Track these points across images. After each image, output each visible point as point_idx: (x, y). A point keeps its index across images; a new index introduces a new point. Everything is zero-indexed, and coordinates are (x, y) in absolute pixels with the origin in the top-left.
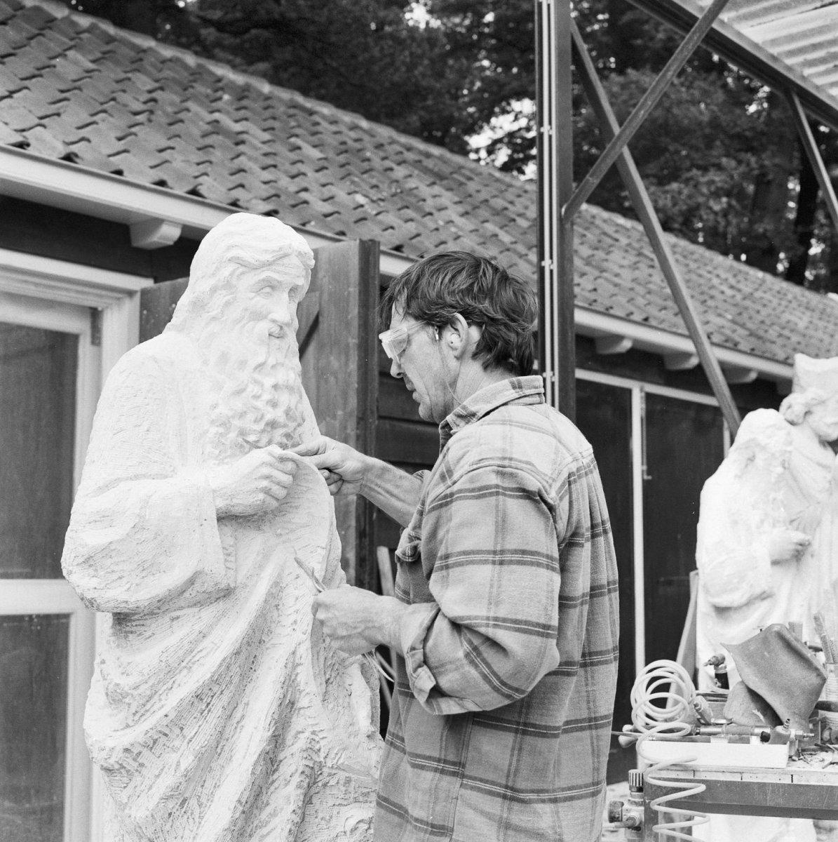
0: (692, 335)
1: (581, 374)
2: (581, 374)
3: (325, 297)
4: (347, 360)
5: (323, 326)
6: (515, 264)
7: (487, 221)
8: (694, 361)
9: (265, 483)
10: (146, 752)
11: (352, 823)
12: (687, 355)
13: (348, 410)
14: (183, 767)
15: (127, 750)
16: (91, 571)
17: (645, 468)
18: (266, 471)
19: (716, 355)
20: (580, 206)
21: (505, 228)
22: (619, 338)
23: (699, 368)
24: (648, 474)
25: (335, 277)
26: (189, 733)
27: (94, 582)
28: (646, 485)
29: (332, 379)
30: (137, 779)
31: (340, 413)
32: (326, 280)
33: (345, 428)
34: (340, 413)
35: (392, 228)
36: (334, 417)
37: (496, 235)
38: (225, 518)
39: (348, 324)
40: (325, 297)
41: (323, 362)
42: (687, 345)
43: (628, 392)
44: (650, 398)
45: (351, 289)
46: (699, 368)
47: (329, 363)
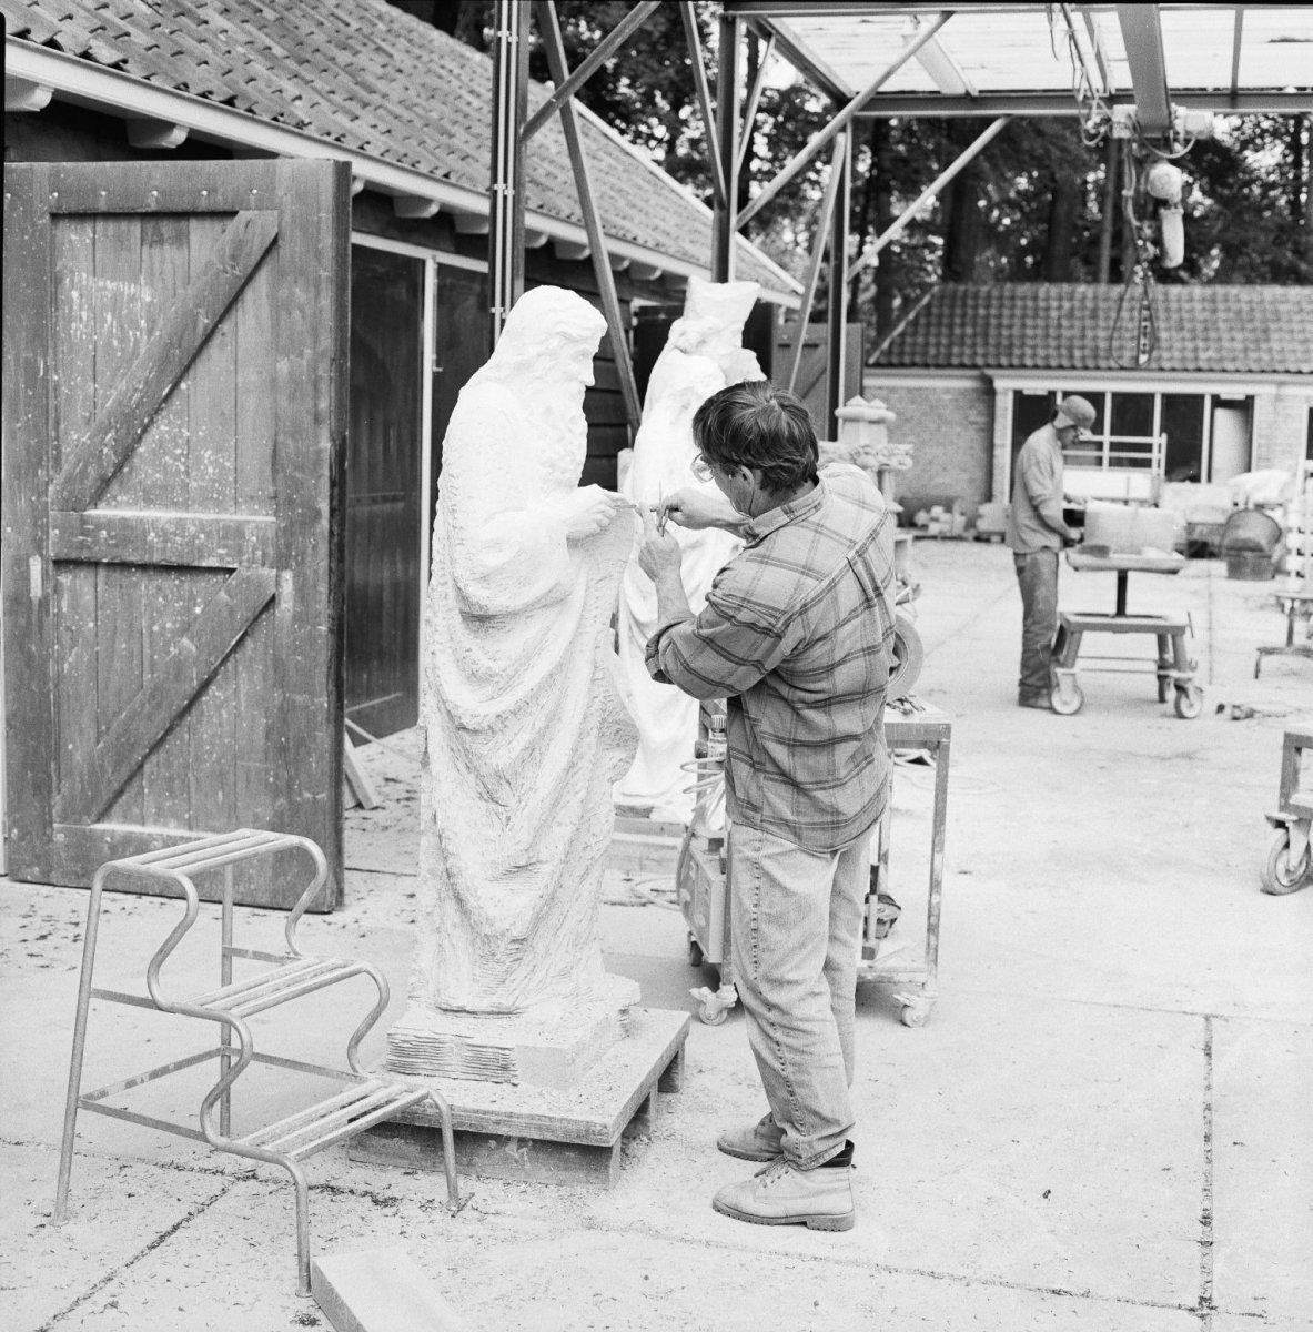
0: (587, 223)
1: (357, 238)
2: (357, 238)
3: (287, 217)
4: (318, 295)
5: (285, 249)
6: (317, 104)
7: (247, 21)
8: (587, 253)
9: (600, 517)
10: (511, 717)
11: (614, 761)
12: (581, 247)
13: (320, 349)
14: (537, 727)
15: (499, 716)
16: (485, 584)
17: (435, 357)
18: (602, 507)
19: (607, 246)
20: (784, 217)
21: (266, 30)
22: (427, 201)
23: (589, 261)
24: (438, 366)
25: (300, 197)
26: (542, 701)
27: (486, 593)
28: (436, 376)
29: (297, 314)
30: (499, 737)
31: (308, 351)
32: (288, 199)
33: (315, 369)
34: (308, 351)
35: (206, 63)
36: (301, 355)
37: (269, 48)
38: (573, 543)
39: (318, 254)
40: (287, 217)
41: (283, 293)
42: (579, 236)
43: (423, 262)
44: (443, 270)
45: (323, 215)
46: (589, 261)
47: (292, 294)
